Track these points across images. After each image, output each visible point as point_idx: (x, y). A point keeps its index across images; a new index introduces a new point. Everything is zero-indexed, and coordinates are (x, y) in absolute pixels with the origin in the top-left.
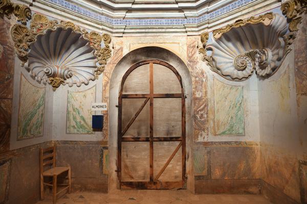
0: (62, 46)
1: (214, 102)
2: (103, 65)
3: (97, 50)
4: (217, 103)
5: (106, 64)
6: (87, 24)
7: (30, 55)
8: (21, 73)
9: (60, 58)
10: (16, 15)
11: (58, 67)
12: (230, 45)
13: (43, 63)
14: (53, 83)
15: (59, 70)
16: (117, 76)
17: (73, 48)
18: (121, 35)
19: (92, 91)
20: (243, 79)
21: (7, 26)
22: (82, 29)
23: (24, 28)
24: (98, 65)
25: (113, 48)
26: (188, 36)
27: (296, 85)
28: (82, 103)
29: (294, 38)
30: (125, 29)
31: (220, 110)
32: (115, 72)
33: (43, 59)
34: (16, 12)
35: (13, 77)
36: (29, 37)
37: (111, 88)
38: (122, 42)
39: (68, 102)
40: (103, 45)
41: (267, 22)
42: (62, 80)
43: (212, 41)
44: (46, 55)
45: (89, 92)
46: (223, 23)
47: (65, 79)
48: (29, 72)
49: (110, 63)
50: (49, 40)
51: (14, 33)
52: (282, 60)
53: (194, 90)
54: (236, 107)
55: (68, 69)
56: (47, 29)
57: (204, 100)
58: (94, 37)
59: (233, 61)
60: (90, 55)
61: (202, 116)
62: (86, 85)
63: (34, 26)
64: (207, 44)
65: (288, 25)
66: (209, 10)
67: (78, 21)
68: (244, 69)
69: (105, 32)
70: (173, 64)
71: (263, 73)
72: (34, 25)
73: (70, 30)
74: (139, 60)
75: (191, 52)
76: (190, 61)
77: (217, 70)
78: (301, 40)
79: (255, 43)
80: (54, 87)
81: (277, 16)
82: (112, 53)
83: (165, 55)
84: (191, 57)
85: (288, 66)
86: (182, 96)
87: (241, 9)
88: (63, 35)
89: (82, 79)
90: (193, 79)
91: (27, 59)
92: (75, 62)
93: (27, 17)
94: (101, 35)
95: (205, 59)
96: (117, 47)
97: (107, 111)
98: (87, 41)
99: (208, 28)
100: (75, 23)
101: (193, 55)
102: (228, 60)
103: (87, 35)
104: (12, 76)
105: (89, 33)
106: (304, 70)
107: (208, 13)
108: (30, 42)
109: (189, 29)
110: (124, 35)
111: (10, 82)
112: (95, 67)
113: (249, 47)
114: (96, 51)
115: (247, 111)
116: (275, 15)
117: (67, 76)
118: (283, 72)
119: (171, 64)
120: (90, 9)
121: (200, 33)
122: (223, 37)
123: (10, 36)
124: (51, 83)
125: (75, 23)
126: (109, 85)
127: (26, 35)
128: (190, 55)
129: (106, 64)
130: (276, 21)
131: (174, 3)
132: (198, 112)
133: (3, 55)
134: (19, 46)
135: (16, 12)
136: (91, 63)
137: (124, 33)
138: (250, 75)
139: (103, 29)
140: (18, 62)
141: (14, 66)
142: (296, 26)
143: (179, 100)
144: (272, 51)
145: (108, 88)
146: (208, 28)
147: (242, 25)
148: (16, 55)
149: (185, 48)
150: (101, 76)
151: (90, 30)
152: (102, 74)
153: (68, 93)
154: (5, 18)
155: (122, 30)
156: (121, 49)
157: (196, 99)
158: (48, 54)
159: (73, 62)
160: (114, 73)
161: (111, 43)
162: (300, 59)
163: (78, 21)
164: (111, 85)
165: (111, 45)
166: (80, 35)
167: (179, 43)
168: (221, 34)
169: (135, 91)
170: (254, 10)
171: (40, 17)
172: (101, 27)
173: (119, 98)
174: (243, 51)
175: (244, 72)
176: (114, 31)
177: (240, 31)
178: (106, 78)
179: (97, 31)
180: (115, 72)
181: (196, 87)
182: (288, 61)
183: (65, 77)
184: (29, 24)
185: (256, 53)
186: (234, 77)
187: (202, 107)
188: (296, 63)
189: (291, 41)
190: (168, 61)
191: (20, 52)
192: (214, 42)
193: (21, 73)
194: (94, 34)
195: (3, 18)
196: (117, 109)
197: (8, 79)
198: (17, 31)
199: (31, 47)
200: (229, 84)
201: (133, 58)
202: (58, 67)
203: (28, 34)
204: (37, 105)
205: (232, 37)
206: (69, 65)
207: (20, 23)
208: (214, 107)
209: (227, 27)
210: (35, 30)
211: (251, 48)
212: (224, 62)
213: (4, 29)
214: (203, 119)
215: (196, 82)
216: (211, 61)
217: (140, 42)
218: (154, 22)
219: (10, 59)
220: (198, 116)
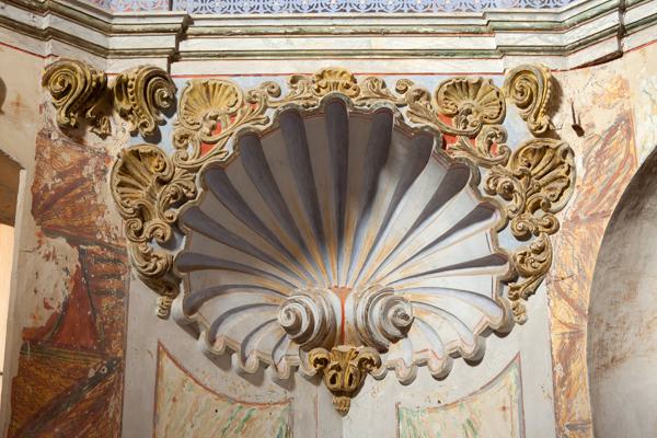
0: (342, 187)
2: (535, 242)
3: (487, 165)
5: (552, 227)
6: (415, 54)
7: (193, 263)
8: (160, 344)
9: (347, 248)
10: (124, 115)
16: (633, 288)
17: (387, 188)
18: (610, 47)
19: (502, 393)
21: (97, 169)
23: (151, 155)
24: (509, 244)
25: (578, 129)
33: (276, 272)
34: (124, 105)
35: (121, 370)
36: (170, 189)
38: (624, 85)
40: (518, 130)
42: (367, 352)
47: (383, 350)
49: (576, 219)
51: (121, 185)
55: (388, 291)
56: (236, 131)
58: (463, 104)
60: (463, 203)
62: (474, 362)
63: (186, 137)
67: (370, 54)
69: (514, 63)
72: (186, 129)
80: (338, 393)
82: (578, 162)
91: (179, 280)
93: (159, 108)
94: (500, 82)
96: (600, 120)
100: (352, 66)
103: (422, 102)
104: (117, 366)
108: (177, 205)
110: (627, 43)
111: (108, 392)
112: (498, 259)
114: (485, 174)
123: (110, 202)
125: (352, 66)
126: (582, 346)
127: (162, 182)
129: (552, 227)
134: (139, 233)
135: (124, 105)
136: (476, 241)
139: (503, 51)
140: (143, 299)
141: (124, 319)
145: (580, 366)
148: (134, 271)
150: (539, 304)
151: (431, 74)
152: (543, 289)
154: (91, 138)
155: (612, 20)
156: (625, 123)
159: (405, 252)
161: (565, 108)
163: (370, 54)
165: (563, 121)
166: (387, 113)
171: (208, 90)
172: (490, 43)
178: (564, 311)
179: (472, 68)
183: (380, 338)
184: (168, 132)
191: (147, 257)
193: (160, 344)
194: (461, 86)
195: (80, 141)
197: (99, 379)
198: (133, 176)
199: (183, 227)
202: (342, 293)
203: (167, 174)
206: (389, 276)
210: (191, 150)
213: (83, 180)
219: (107, 293)
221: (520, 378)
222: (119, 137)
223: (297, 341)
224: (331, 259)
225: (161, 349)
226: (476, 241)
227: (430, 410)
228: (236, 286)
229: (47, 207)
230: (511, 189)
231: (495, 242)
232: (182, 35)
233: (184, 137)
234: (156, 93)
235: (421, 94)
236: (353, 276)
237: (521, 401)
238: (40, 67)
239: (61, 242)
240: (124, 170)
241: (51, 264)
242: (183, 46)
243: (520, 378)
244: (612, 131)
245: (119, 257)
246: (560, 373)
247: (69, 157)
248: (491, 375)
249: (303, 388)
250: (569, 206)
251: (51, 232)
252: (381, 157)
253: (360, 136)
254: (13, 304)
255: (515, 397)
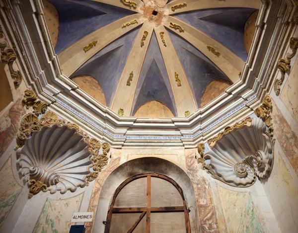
0: (59, 149)
1: (222, 210)
2: (97, 172)
3: (94, 155)
4: (226, 211)
5: (100, 171)
8: (11, 155)
10: (34, 108)
11: (45, 171)
12: (226, 153)
13: (32, 160)
14: (33, 187)
15: (46, 174)
17: (69, 153)
18: (120, 147)
20: (248, 185)
22: (84, 133)
23: (36, 117)
24: (91, 170)
26: (185, 148)
27: (290, 163)
28: (61, 213)
29: (273, 130)
30: (124, 142)
31: (231, 219)
32: (109, 181)
37: (101, 198)
39: (43, 211)
40: (101, 152)
41: (249, 124)
43: (208, 149)
44: (39, 154)
45: (74, 200)
46: (215, 133)
48: (17, 159)
49: (105, 171)
50: (116, 48)
52: (273, 152)
53: (197, 197)
54: (248, 214)
55: (56, 174)
57: (209, 208)
59: (233, 169)
61: (210, 227)
64: (204, 153)
65: (264, 123)
66: (202, 128)
67: (83, 127)
68: (247, 174)
70: (173, 176)
71: (261, 175)
73: (74, 130)
74: (135, 173)
75: (190, 162)
76: (190, 170)
77: (219, 176)
78: (277, 129)
79: (248, 149)
81: (254, 119)
82: (109, 162)
83: (163, 167)
84: (191, 166)
85: (279, 153)
86: (184, 210)
87: (227, 120)
88: (67, 133)
89: (69, 185)
90: (195, 186)
92: (67, 169)
95: (205, 168)
96: (114, 157)
97: (92, 222)
98: (86, 145)
99: (204, 140)
101: (192, 164)
102: (228, 169)
105: (90, 138)
106: (290, 148)
107: (201, 130)
108: (34, 130)
109: (186, 143)
110: (123, 148)
113: (244, 154)
114: (93, 156)
115: (264, 219)
116: (253, 118)
117: (52, 181)
118: (277, 161)
119: (170, 177)
120: (95, 122)
121: (196, 146)
122: (217, 145)
123: (21, 120)
124: (31, 185)
126: (99, 192)
127: (35, 123)
128: (189, 164)
129: (100, 171)
130: (255, 121)
131: (170, 123)
132: (205, 221)
133: (7, 130)
134: (23, 130)
136: (84, 169)
137: (123, 145)
138: (253, 181)
139: (103, 139)
140: (14, 144)
142: (270, 122)
143: (181, 215)
144: (264, 151)
145: (98, 195)
146: (203, 140)
147: (231, 130)
149: (184, 159)
151: (92, 136)
152: (94, 181)
153: (47, 201)
154: (25, 107)
155: (123, 143)
156: (119, 159)
157: (201, 206)
158: (41, 155)
159: (64, 168)
160: (106, 183)
162: (284, 141)
163: (83, 127)
164: (101, 194)
166: (82, 137)
167: (177, 155)
168: (215, 142)
169: (129, 205)
170: (237, 119)
171: (53, 114)
172: (102, 137)
173: (108, 212)
174: (241, 160)
175: (247, 178)
176: (114, 143)
177: (230, 137)
178: (97, 185)
179: (98, 139)
180: (109, 181)
181: (199, 194)
182: (277, 149)
184: (40, 117)
185: (252, 158)
186: (238, 183)
187: (209, 215)
188: (282, 146)
189: (272, 133)
190: (166, 174)
192: (210, 150)
193: (11, 155)
194: (95, 140)
195: (23, 106)
196: (103, 227)
198: (28, 119)
200: (234, 190)
201: (129, 169)
202: (45, 171)
204: (6, 200)
205: (226, 146)
206: (58, 171)
207: (34, 114)
208: (223, 215)
209: (219, 135)
211: (246, 155)
212: (225, 171)
214: (213, 230)
215: (199, 189)
216: (210, 169)
217: (139, 153)
218: (153, 138)
219: (10, 137)
220: (206, 227)
221: (83, 196)
222: (30, 110)
223: (30, 175)
224: (46, 162)
225: (10, 156)
226: (84, 169)
227: (57, 200)
228: (27, 156)
229: (12, 112)
230: (96, 161)
231: (89, 169)
232: (52, 103)
233: (44, 119)
234: (43, 108)
235: (88, 137)
236: (49, 168)
237: (82, 201)
238: (26, 89)
239: (10, 120)
240: (28, 117)
241: (6, 122)
242: (51, 105)
243: (83, 196)
244: (116, 159)
245: (15, 132)
246: (93, 196)
247: (20, 107)
248: (76, 195)
249: (26, 186)
250: (105, 168)
251: (10, 116)
252: (72, 146)
253: (73, 139)
254: (147, 69)
255: (81, 199)
